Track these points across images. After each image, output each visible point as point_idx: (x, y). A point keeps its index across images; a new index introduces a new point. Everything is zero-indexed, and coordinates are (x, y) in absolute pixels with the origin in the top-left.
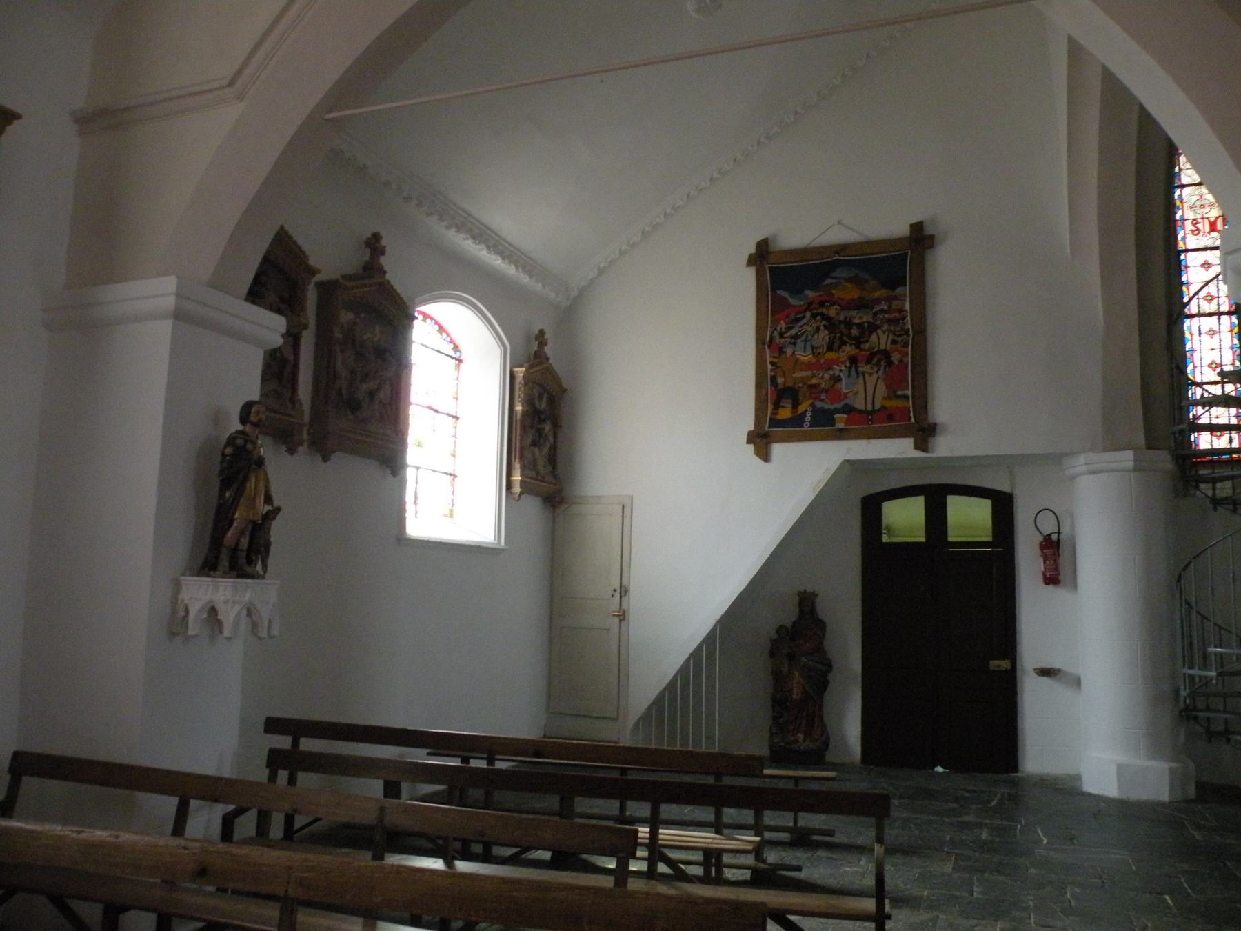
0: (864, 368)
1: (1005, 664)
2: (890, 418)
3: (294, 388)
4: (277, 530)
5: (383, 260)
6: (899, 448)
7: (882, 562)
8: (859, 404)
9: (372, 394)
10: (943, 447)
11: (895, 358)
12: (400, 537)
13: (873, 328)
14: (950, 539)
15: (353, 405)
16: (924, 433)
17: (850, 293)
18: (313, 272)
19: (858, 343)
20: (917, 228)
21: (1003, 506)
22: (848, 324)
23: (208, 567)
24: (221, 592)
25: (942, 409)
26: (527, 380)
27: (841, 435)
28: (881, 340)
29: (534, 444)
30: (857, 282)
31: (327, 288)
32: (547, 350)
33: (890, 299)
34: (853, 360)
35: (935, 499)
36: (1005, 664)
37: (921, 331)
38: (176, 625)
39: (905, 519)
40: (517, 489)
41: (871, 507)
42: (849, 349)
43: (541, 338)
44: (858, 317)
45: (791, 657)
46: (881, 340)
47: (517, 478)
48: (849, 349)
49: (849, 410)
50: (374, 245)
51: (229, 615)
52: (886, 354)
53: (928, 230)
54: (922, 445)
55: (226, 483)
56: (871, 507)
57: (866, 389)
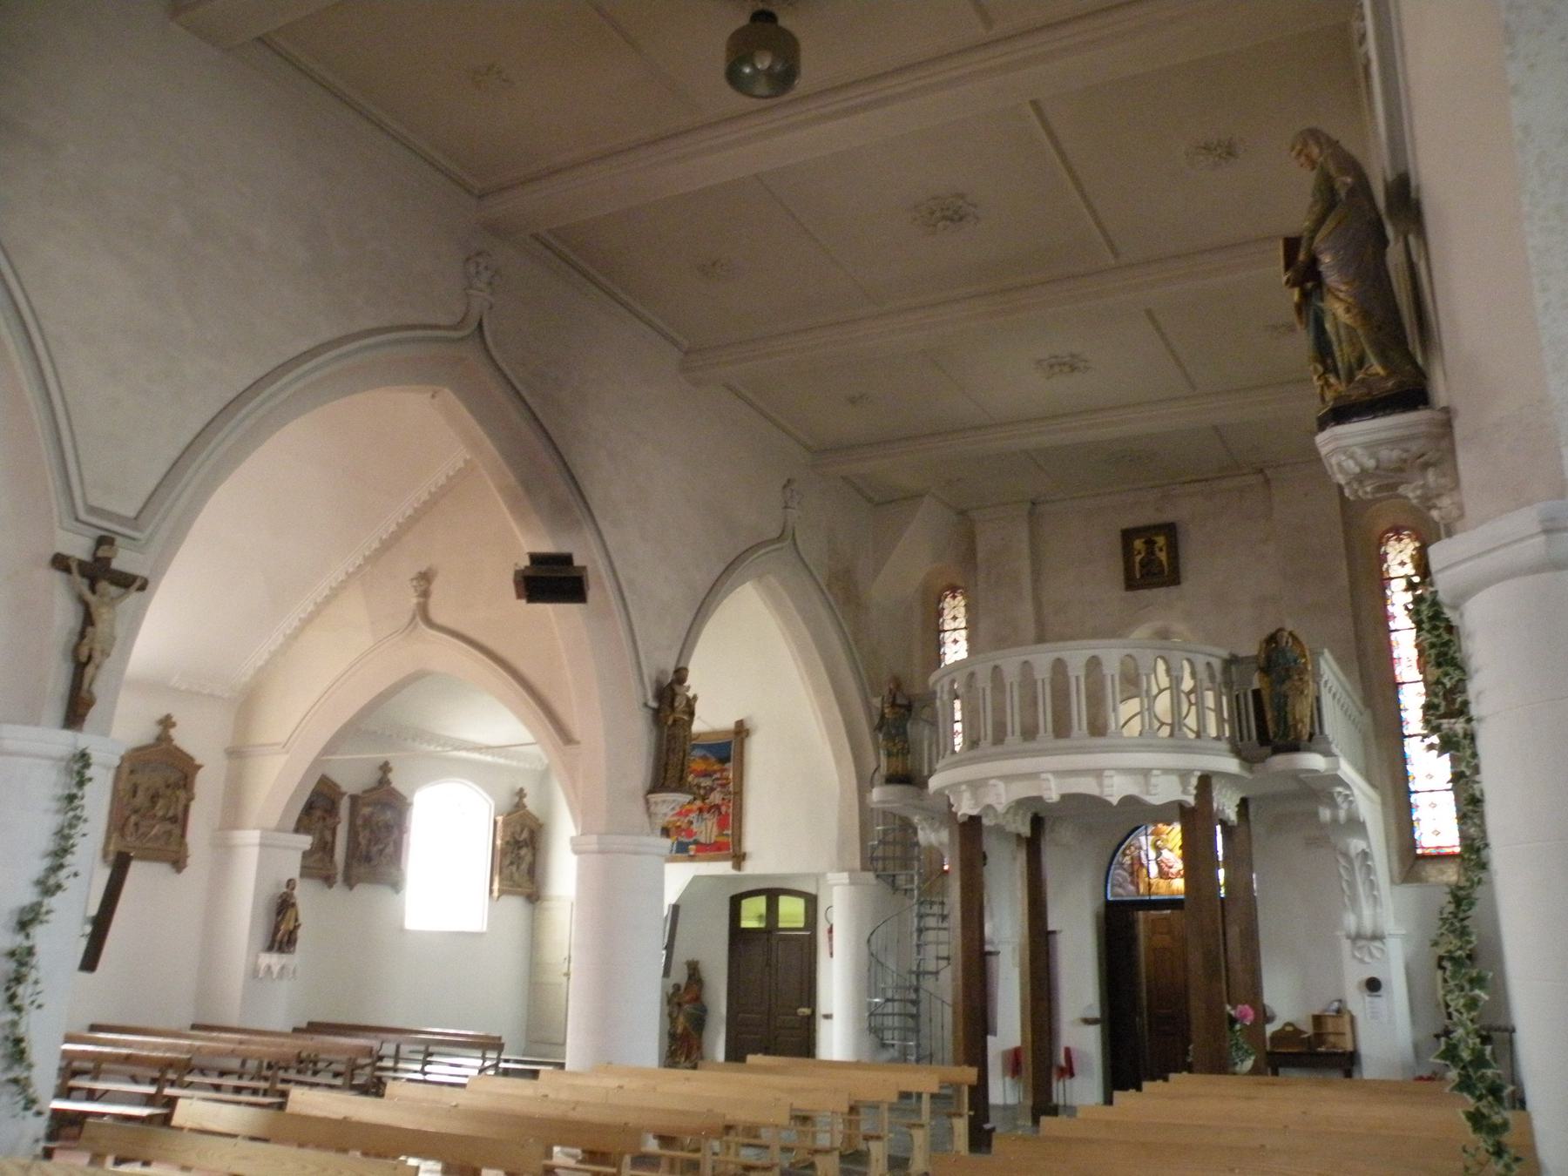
0: (706, 815)
1: (805, 1011)
2: (719, 849)
3: (332, 856)
4: (300, 933)
5: (391, 776)
6: (723, 868)
7: (738, 937)
8: (702, 839)
9: (381, 851)
10: (750, 868)
11: (723, 809)
12: (402, 930)
13: (712, 789)
14: (781, 925)
15: (368, 859)
16: (739, 859)
17: (699, 765)
18: (343, 794)
19: (704, 799)
20: (740, 724)
21: (811, 902)
22: (699, 787)
23: (270, 949)
24: (274, 960)
25: (749, 844)
26: (505, 824)
27: (692, 859)
28: (716, 798)
29: (512, 863)
30: (704, 758)
31: (354, 799)
32: (525, 800)
33: (723, 770)
34: (701, 810)
35: (772, 895)
36: (805, 1011)
37: (739, 794)
38: (254, 973)
39: (753, 914)
40: (496, 894)
41: (735, 903)
42: (698, 803)
43: (521, 793)
44: (706, 782)
45: (679, 1005)
46: (716, 798)
47: (496, 886)
48: (698, 803)
49: (696, 842)
50: (385, 768)
51: (276, 969)
52: (718, 807)
53: (748, 725)
54: (738, 866)
55: (278, 914)
56: (735, 903)
57: (706, 829)
